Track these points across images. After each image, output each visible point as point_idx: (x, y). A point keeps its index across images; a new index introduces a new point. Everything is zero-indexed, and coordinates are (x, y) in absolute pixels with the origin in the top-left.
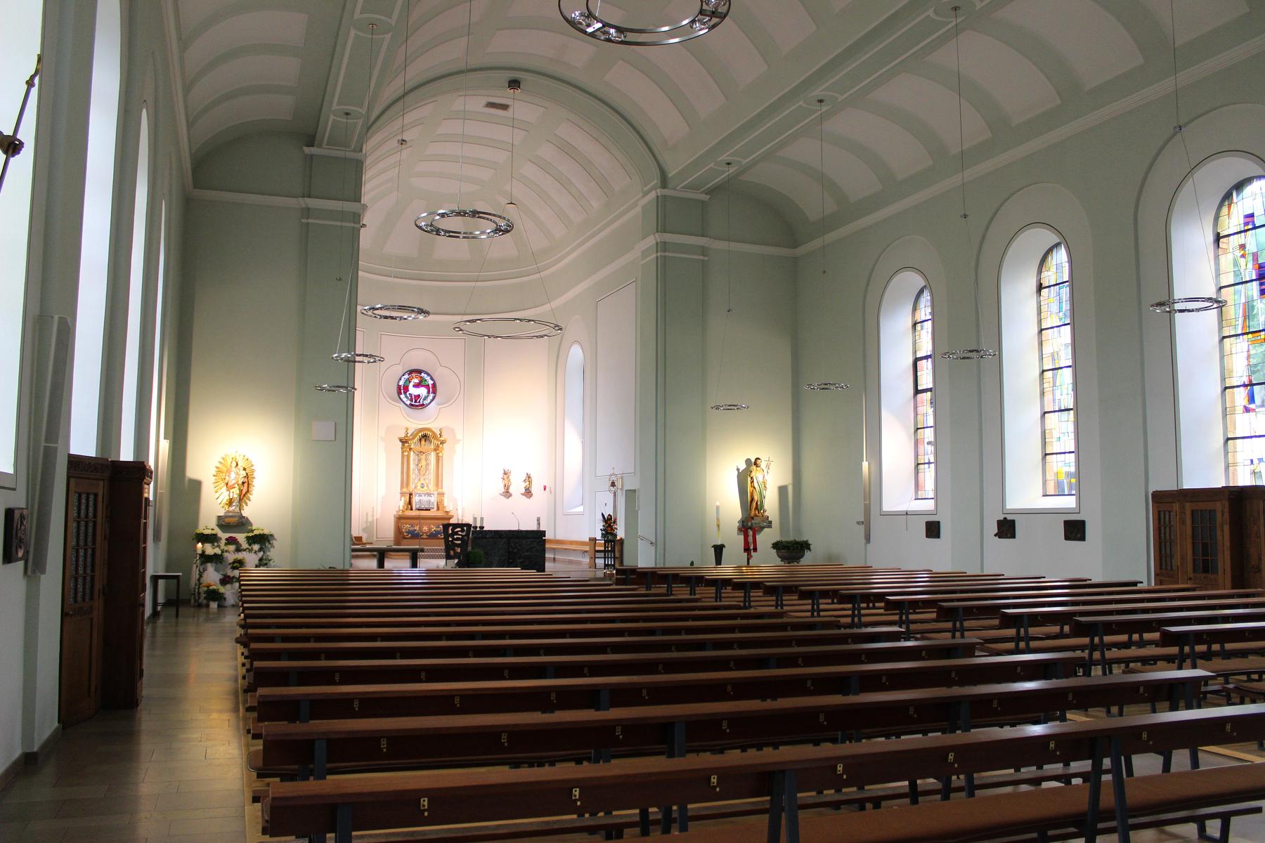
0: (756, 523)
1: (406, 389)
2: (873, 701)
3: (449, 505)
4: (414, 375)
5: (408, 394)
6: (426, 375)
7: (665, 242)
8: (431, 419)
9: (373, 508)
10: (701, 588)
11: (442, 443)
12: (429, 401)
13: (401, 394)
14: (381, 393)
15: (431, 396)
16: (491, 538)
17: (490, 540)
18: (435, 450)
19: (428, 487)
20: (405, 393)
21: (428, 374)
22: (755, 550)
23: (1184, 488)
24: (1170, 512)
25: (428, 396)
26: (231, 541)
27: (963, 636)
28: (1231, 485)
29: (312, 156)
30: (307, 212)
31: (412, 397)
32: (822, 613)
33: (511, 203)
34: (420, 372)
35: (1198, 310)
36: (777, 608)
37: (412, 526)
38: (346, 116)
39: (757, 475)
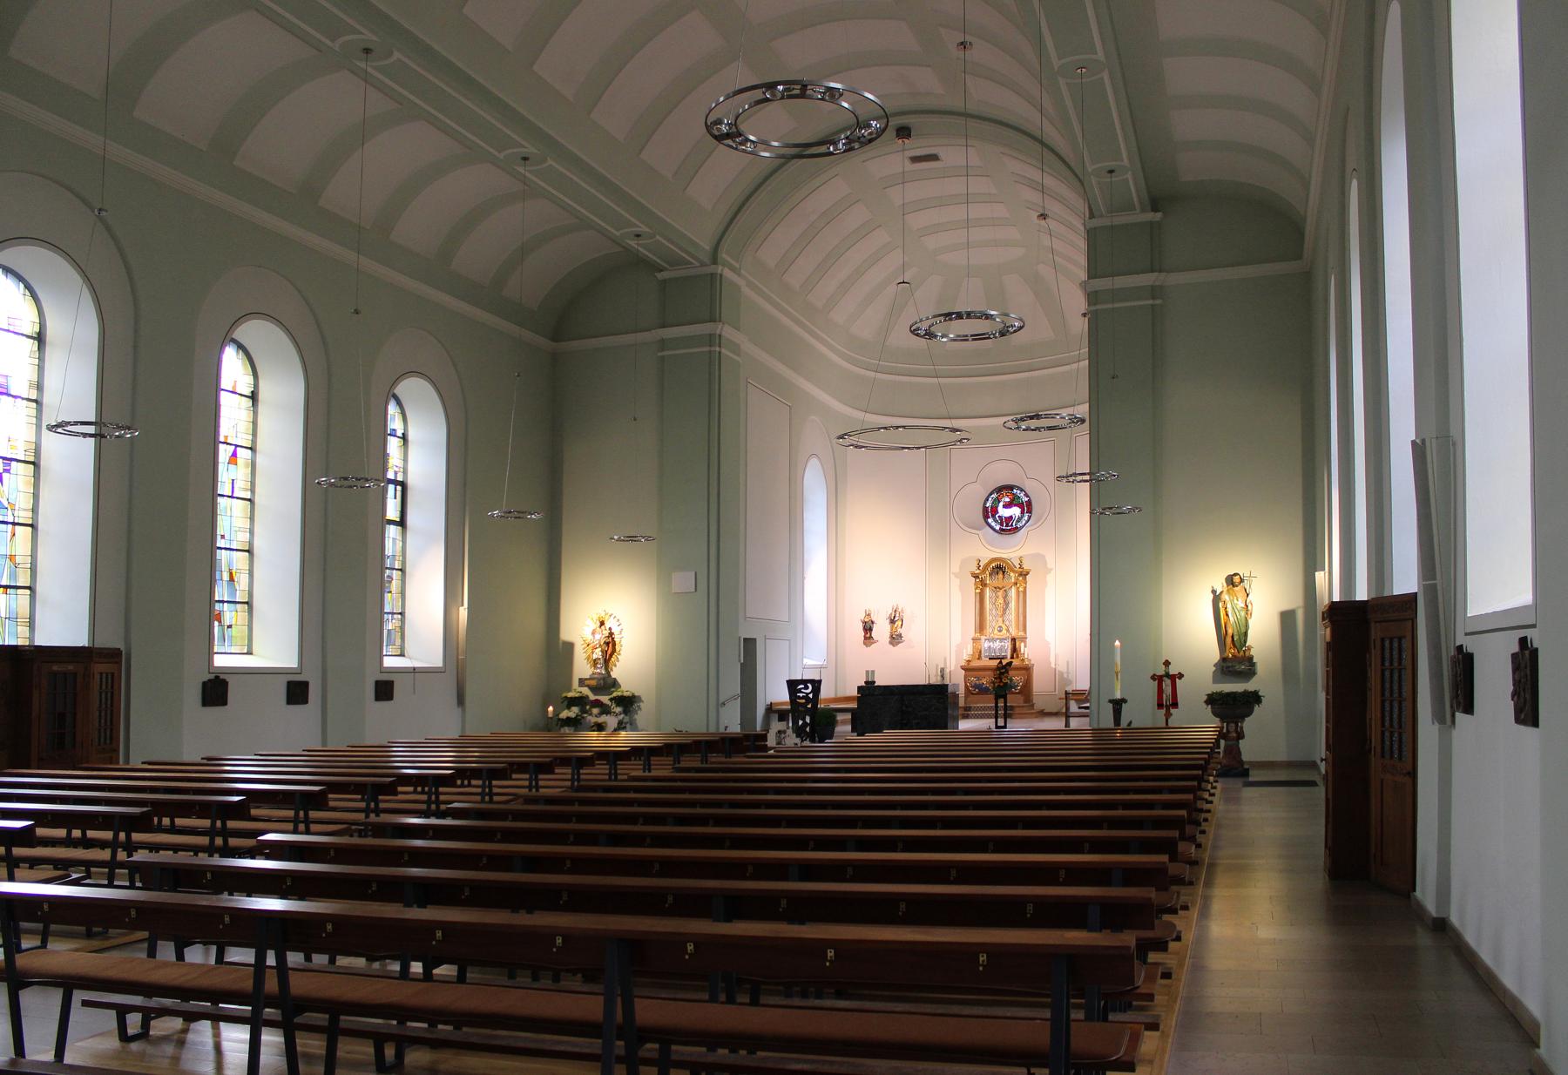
0: (1229, 667)
1: (995, 510)
3: (1028, 651)
4: (1004, 492)
6: (1019, 492)
7: (1096, 292)
8: (1011, 550)
9: (945, 659)
10: (632, 762)
11: (1024, 574)
12: (1024, 522)
16: (881, 695)
19: (1008, 631)
20: (993, 516)
21: (1022, 490)
22: (1175, 705)
23: (1357, 599)
24: (1400, 639)
25: (1022, 517)
26: (597, 703)
28: (6, 644)
29: (665, 281)
30: (663, 344)
31: (1002, 520)
32: (496, 798)
33: (904, 282)
34: (1011, 488)
35: (76, 423)
36: (530, 790)
38: (1109, 175)
39: (1233, 604)
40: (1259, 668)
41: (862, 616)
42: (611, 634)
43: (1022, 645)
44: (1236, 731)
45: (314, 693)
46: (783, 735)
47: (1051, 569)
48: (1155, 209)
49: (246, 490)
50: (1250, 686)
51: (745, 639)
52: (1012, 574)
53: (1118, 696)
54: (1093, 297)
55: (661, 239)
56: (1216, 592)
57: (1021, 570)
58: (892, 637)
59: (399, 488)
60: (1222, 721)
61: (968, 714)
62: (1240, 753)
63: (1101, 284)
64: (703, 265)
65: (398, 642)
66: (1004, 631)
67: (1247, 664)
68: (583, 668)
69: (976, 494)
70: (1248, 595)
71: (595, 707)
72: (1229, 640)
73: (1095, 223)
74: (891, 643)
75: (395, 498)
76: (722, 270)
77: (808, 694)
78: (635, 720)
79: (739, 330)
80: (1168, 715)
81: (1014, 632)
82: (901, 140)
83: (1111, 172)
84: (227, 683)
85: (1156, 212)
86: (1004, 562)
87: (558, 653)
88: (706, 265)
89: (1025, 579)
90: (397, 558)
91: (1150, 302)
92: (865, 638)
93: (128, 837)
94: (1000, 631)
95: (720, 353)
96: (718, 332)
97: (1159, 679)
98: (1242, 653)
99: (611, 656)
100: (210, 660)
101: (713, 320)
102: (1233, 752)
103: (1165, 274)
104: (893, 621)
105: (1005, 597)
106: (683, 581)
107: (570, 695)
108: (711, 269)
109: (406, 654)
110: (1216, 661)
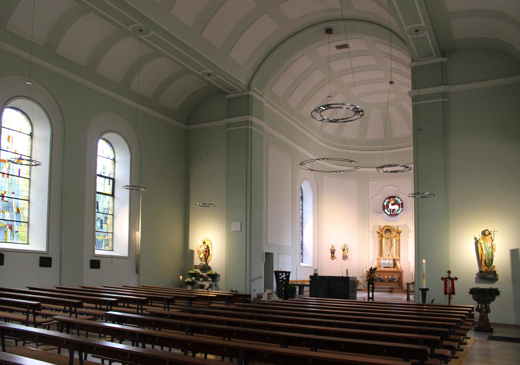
1: (388, 206)
2: (414, 345)
4: (391, 199)
5: (388, 209)
6: (398, 199)
9: (366, 267)
11: (399, 233)
12: (400, 211)
13: (385, 209)
14: (369, 209)
15: (401, 209)
17: (319, 281)
18: (395, 237)
19: (392, 256)
20: (387, 209)
21: (399, 198)
22: (453, 293)
25: (399, 209)
26: (202, 276)
27: (169, 310)
30: (228, 125)
33: (330, 97)
34: (394, 197)
37: (379, 275)
38: (208, 76)
39: (485, 245)
40: (500, 277)
41: (330, 247)
42: (208, 247)
43: (398, 262)
44: (486, 308)
45: (55, 262)
46: (270, 296)
47: (411, 231)
48: (443, 56)
49: (27, 174)
50: (494, 286)
51: (266, 253)
52: (393, 232)
53: (424, 287)
54: (415, 99)
55: (219, 76)
56: (477, 238)
57: (397, 231)
58: (343, 257)
59: (111, 181)
60: (478, 302)
61: (390, 289)
62: (488, 320)
63: (416, 92)
64: (244, 91)
65: (110, 245)
66: (391, 256)
67: (493, 274)
68: (197, 261)
69: (379, 199)
70: (493, 241)
71: (201, 278)
72: (483, 262)
73: (415, 64)
74: (343, 259)
75: (109, 184)
76: (252, 94)
77: (283, 278)
78: (218, 284)
79: (263, 121)
80: (450, 298)
81: (395, 257)
82: (327, 35)
83: (417, 31)
84: (4, 255)
85: (444, 57)
86: (391, 228)
87: (188, 254)
88: (245, 91)
89: (399, 235)
90: (110, 210)
91: (442, 100)
92: (332, 256)
93: (142, 307)
94: (389, 256)
95: (251, 129)
96: (250, 120)
97: (445, 280)
98: (490, 269)
99: (208, 256)
100: (94, 252)
101: (248, 114)
102: (484, 318)
103: (449, 86)
104: (344, 250)
105: (391, 242)
106: (236, 226)
107: (191, 272)
108: (248, 93)
109: (29, 244)
110: (477, 272)
